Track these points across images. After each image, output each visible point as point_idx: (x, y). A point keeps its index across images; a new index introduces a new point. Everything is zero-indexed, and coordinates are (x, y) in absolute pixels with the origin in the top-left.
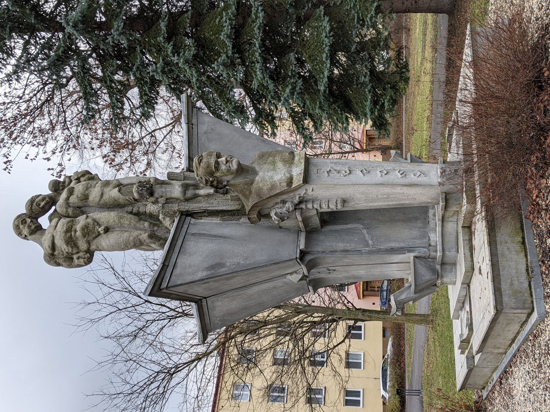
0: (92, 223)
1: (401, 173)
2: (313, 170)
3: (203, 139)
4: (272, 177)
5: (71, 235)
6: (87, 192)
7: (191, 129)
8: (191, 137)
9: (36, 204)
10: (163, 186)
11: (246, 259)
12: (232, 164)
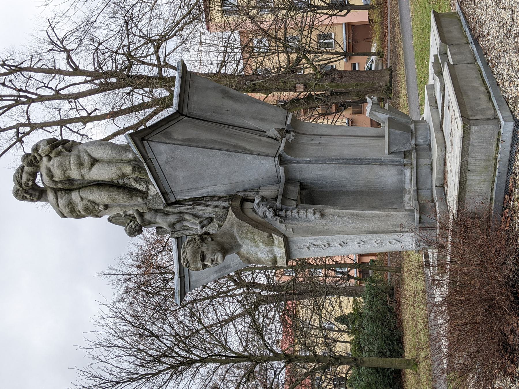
1: (377, 242)
3: (167, 170)
7: (150, 164)
8: (155, 174)
9: (25, 186)
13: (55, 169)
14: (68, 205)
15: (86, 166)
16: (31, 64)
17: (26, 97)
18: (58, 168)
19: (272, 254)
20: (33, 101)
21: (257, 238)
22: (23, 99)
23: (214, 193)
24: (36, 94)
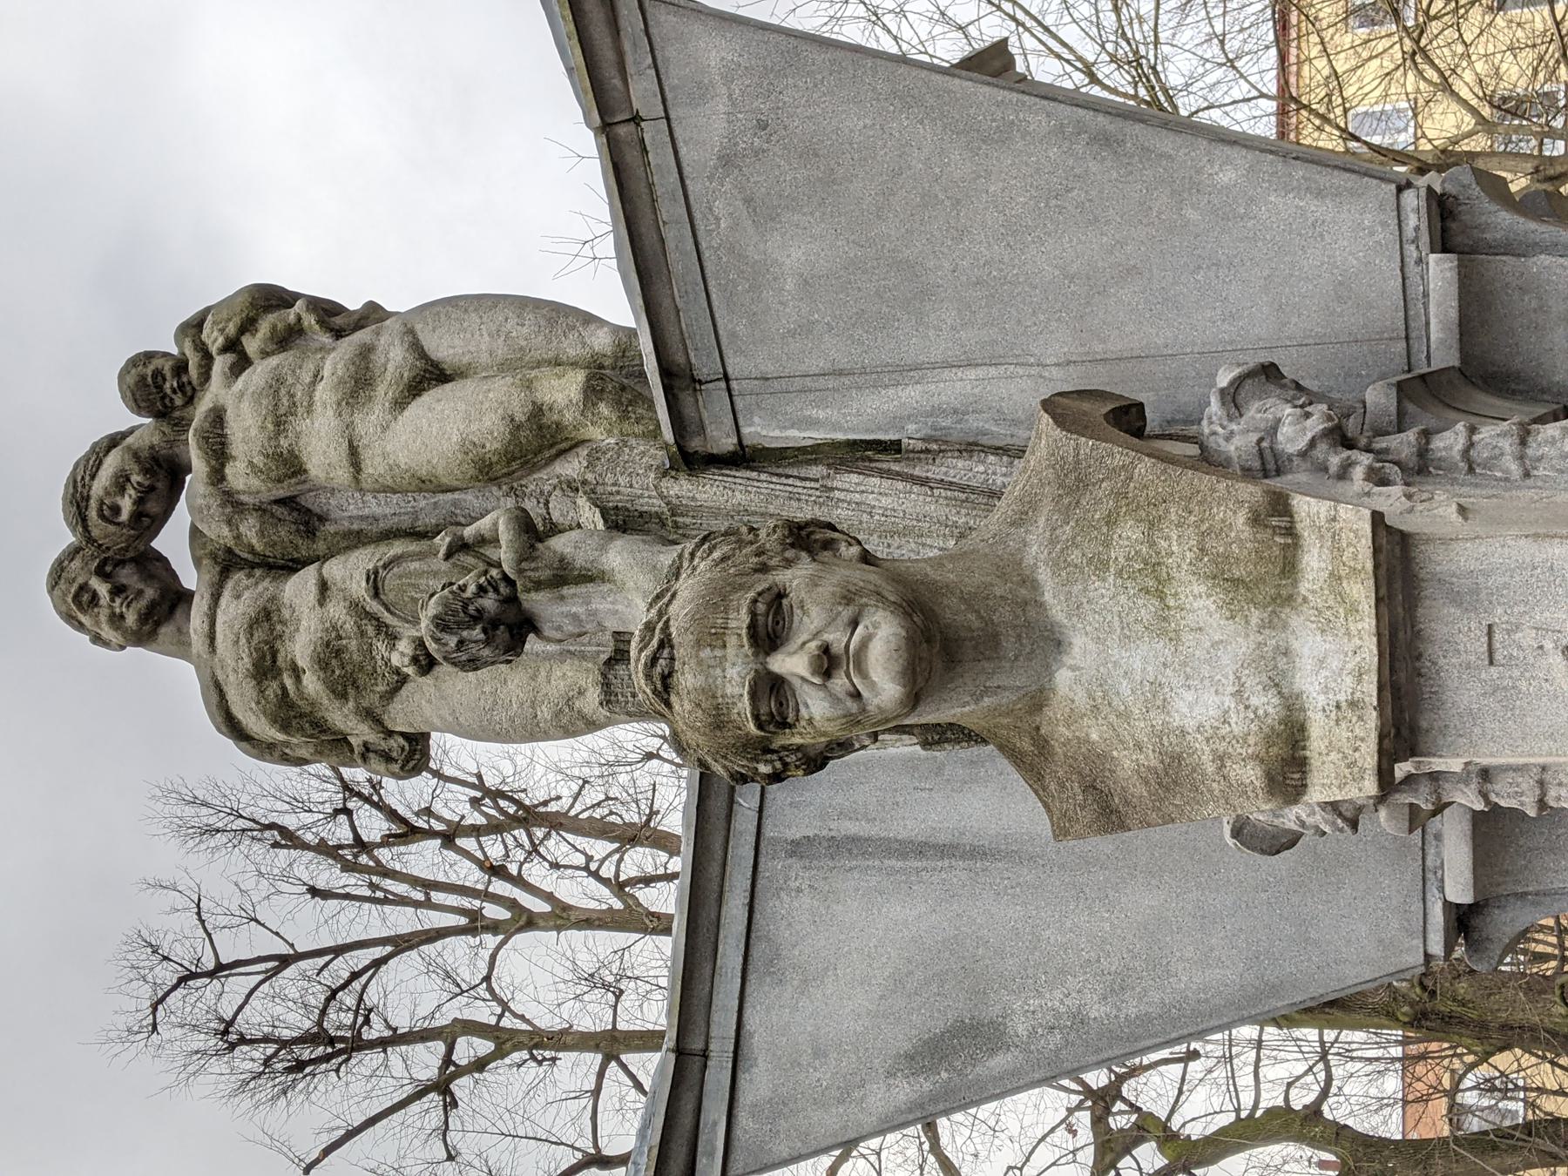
0: (349, 626)
2: (1453, 637)
3: (720, 207)
4: (1157, 698)
5: (284, 688)
6: (284, 443)
7: (631, 156)
9: (101, 516)
10: (565, 591)
11: (1117, 988)
12: (864, 674)
13: (245, 406)
14: (253, 625)
15: (384, 391)
16: (572, 806)
17: (512, 904)
18: (258, 402)
19: (1275, 684)
20: (527, 922)
21: (1178, 548)
22: (493, 912)
23: (974, 423)
24: (549, 897)
